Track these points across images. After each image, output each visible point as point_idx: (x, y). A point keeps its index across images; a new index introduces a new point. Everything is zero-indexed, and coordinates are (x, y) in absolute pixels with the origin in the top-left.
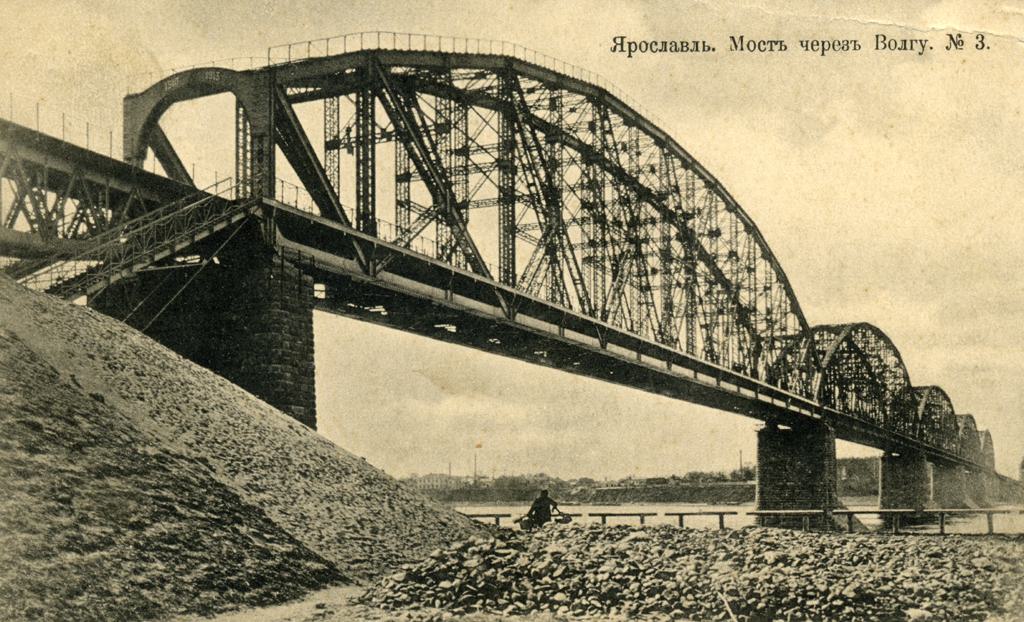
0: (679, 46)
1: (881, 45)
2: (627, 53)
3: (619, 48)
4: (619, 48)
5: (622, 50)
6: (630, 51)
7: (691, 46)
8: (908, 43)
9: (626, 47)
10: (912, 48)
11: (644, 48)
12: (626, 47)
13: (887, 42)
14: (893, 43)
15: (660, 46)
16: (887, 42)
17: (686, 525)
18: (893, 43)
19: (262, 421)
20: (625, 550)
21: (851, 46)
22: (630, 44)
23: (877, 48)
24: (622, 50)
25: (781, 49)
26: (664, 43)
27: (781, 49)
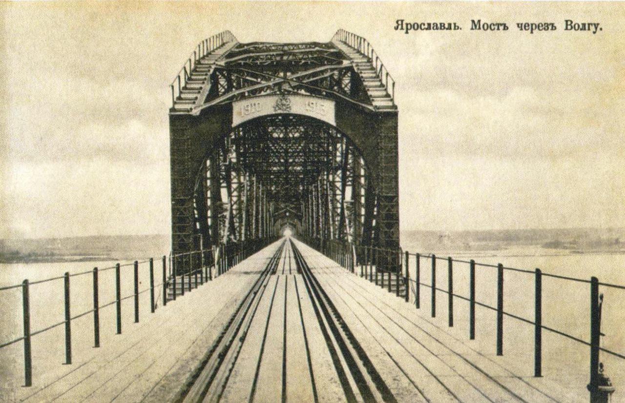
1: (569, 27)
2: (405, 31)
3: (400, 27)
4: (400, 27)
8: (587, 26)
9: (404, 26)
10: (589, 29)
11: (416, 27)
12: (404, 26)
13: (573, 25)
14: (577, 26)
15: (426, 26)
16: (573, 25)
18: (577, 26)
22: (407, 24)
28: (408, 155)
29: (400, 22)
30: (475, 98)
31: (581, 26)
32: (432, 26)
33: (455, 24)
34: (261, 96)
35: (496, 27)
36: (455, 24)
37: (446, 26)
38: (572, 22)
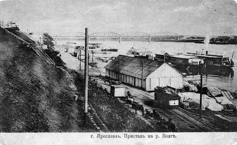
0: (113, 136)
1: (164, 137)
2: (128, 138)
3: (99, 137)
4: (99, 137)
5: (99, 137)
6: (128, 138)
7: (115, 136)
8: (170, 136)
9: (100, 136)
10: (171, 137)
11: (104, 136)
12: (100, 136)
13: (165, 136)
14: (167, 136)
15: (108, 136)
16: (165, 136)
17: (47, 46)
18: (167, 136)
19: (100, 49)
20: (164, 88)
21: (143, 137)
22: (101, 136)
23: (91, 137)
24: (99, 137)
25: (174, 137)
26: (169, 136)
27: (174, 137)
28: (12, 97)
29: (99, 135)
30: (55, 70)
31: (168, 136)
32: (150, 136)
33: (144, 136)
34: (168, 64)
35: (136, 137)
36: (144, 136)
37: (115, 136)
38: (165, 135)
